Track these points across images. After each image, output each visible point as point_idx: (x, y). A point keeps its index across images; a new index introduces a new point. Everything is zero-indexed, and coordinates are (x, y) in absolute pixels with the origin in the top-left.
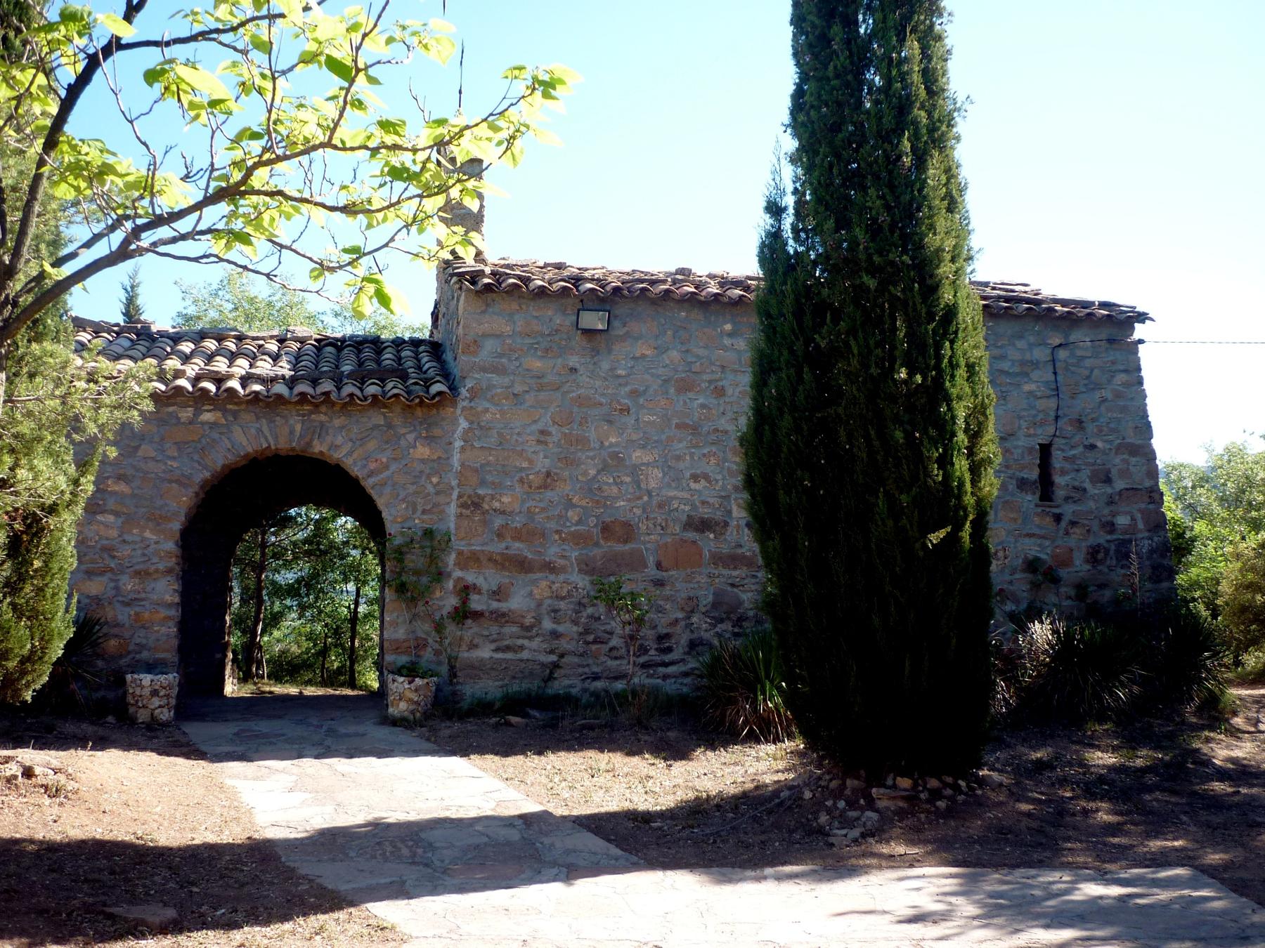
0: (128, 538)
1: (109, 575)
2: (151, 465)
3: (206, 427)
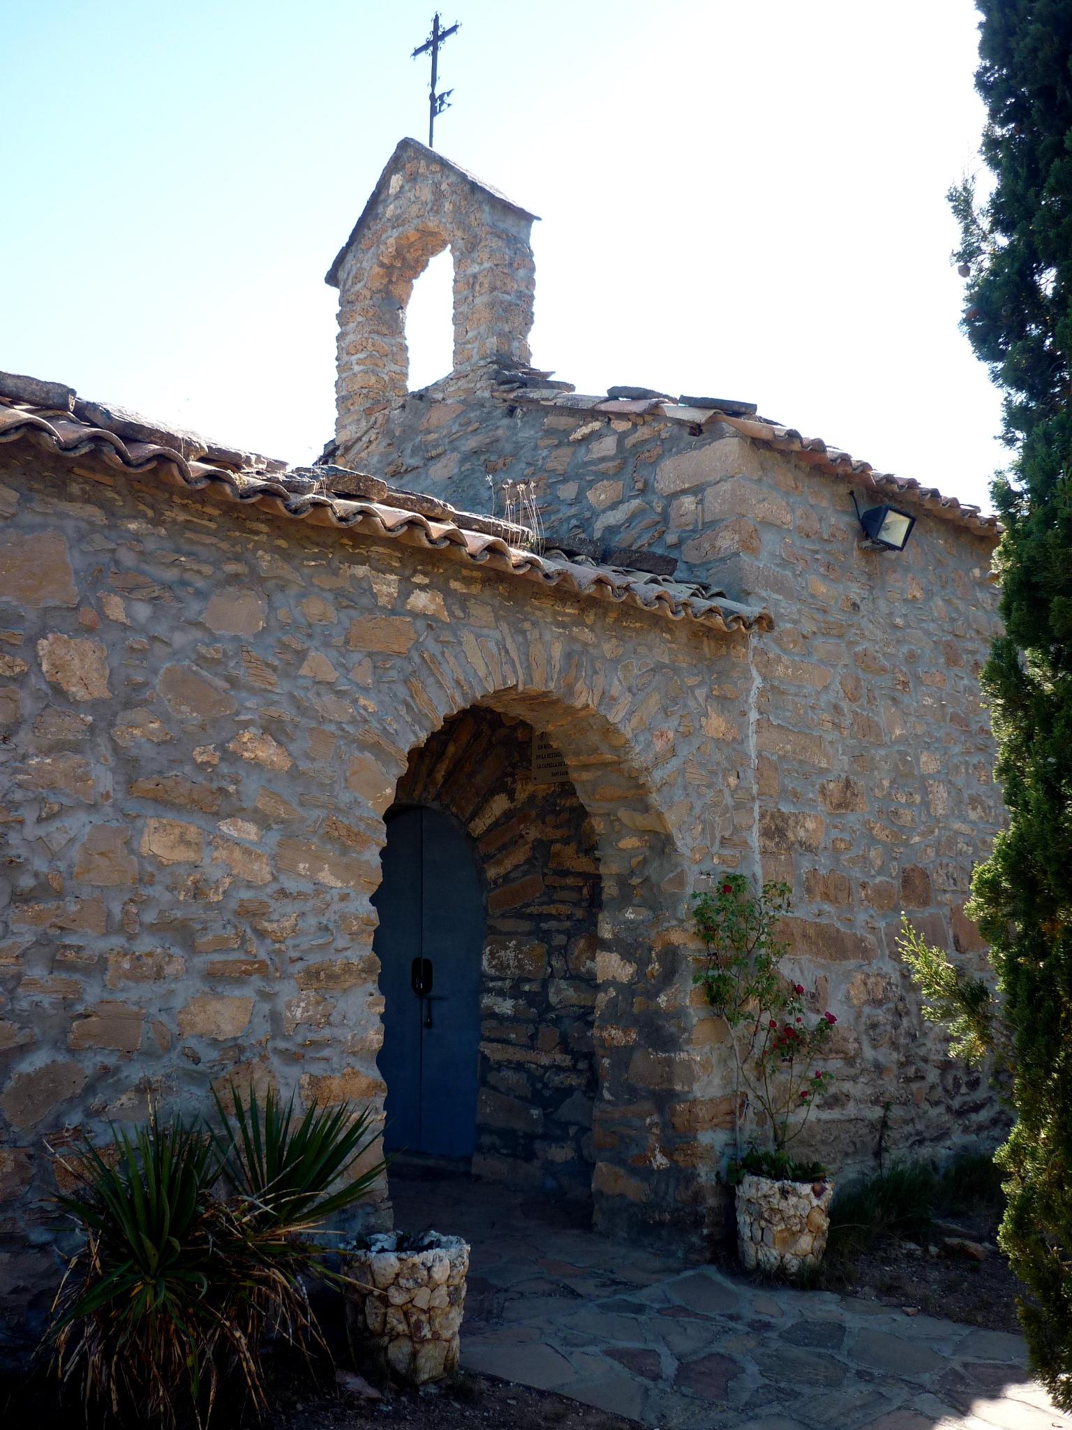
0: (291, 885)
1: (256, 981)
2: (329, 699)
3: (421, 624)
